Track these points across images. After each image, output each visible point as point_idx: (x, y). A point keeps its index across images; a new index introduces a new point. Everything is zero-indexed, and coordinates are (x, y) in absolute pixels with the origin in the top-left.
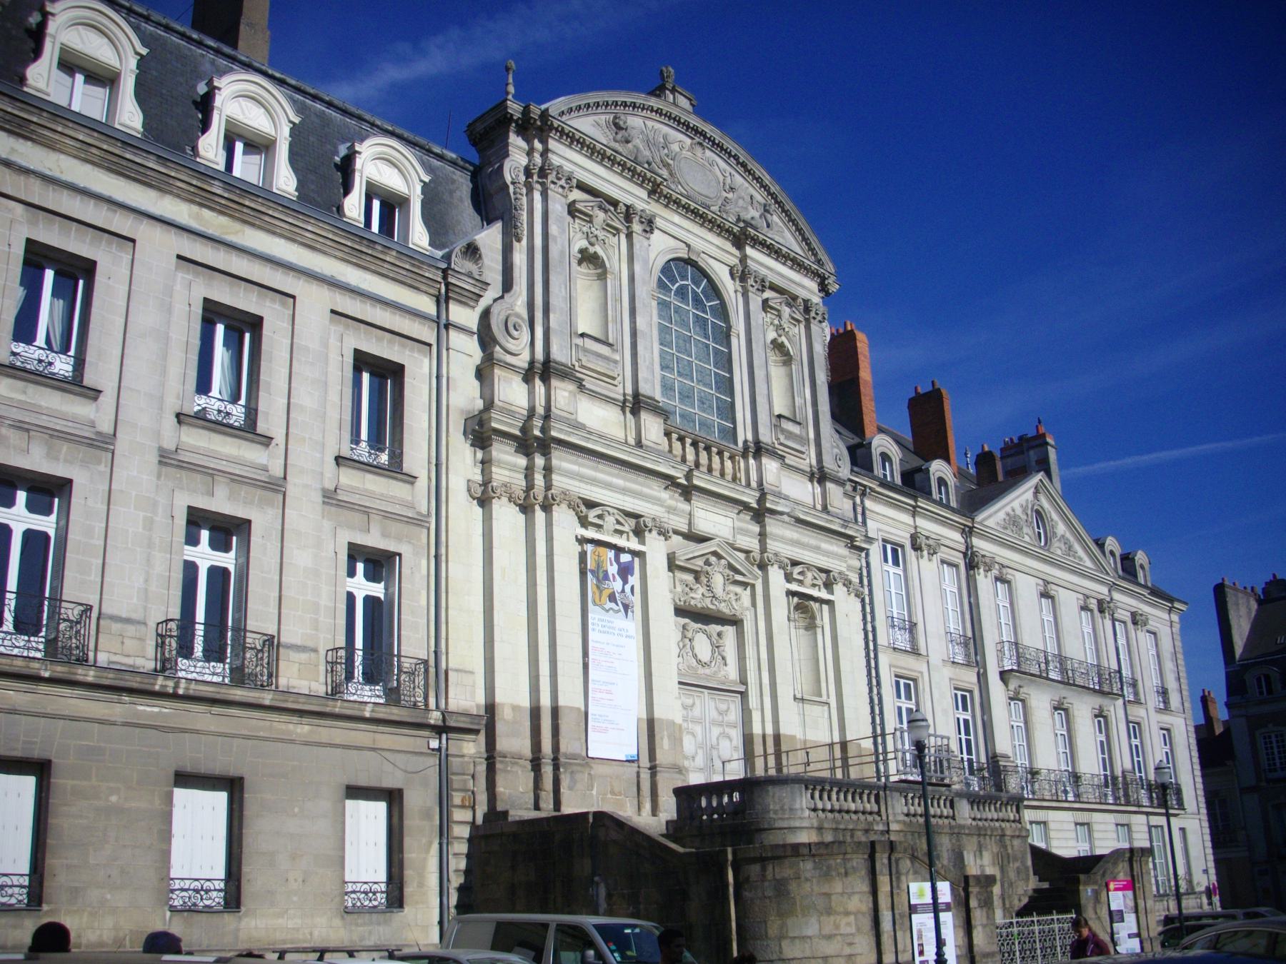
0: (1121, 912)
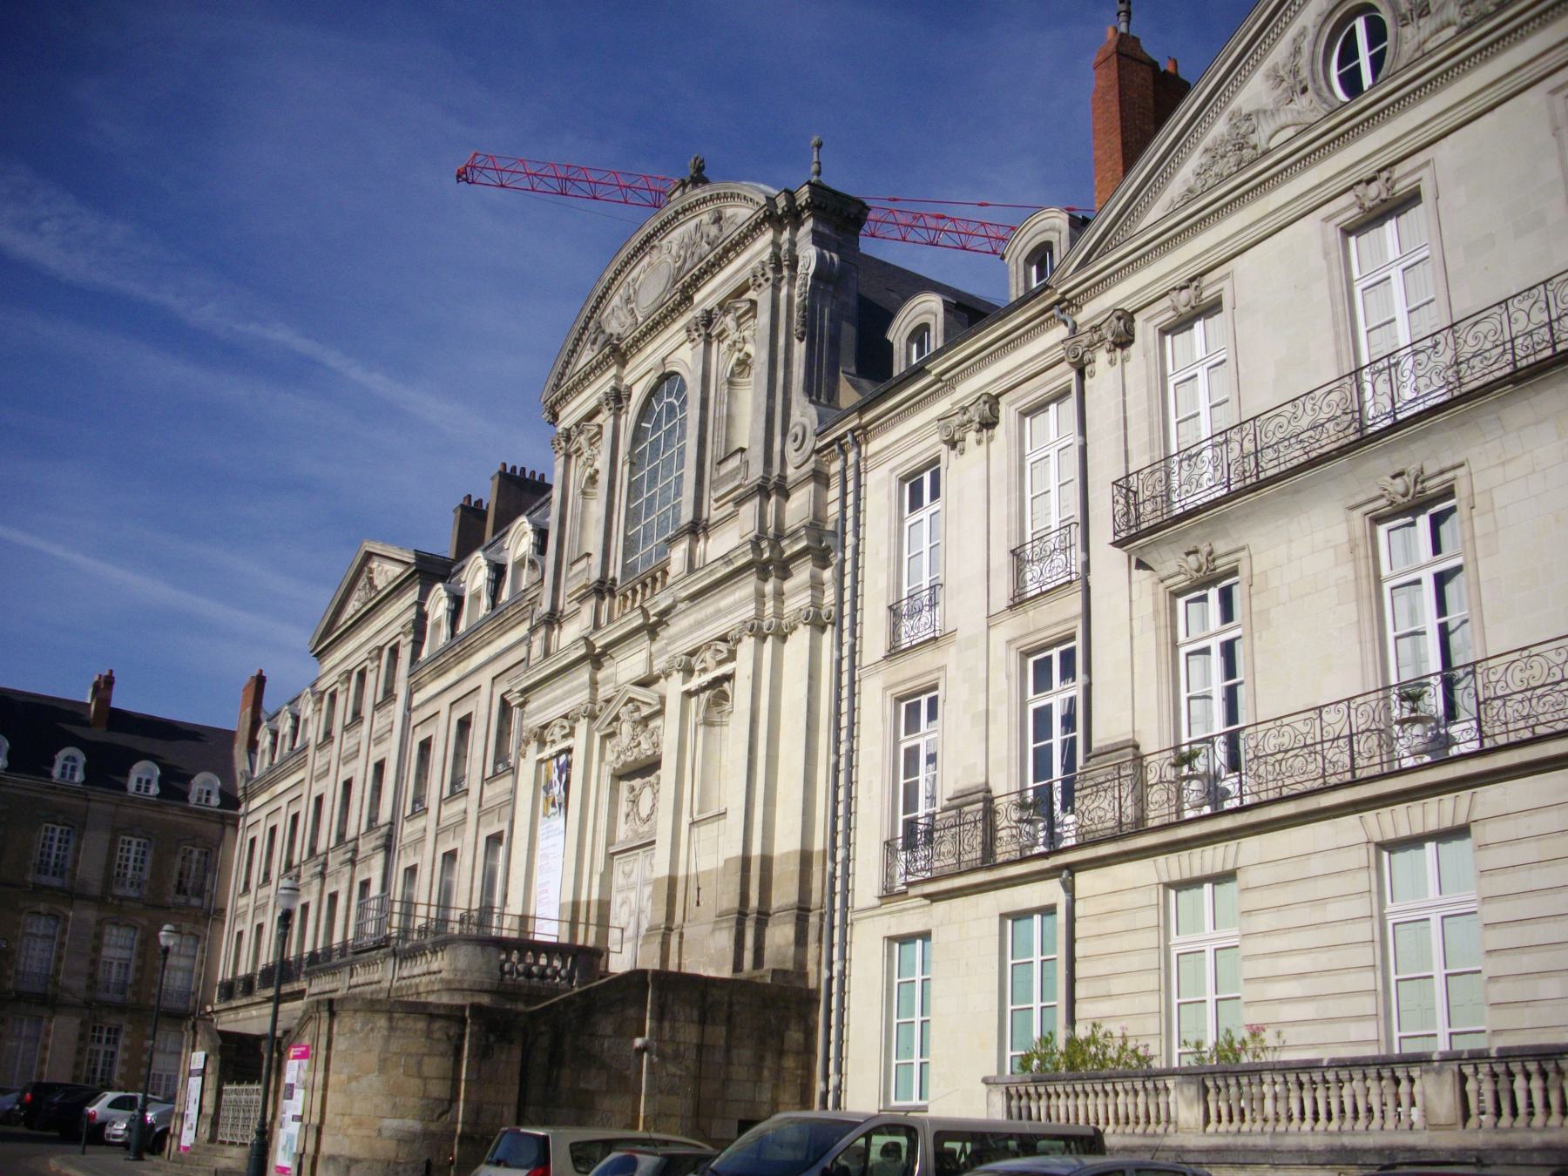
0: (292, 1086)
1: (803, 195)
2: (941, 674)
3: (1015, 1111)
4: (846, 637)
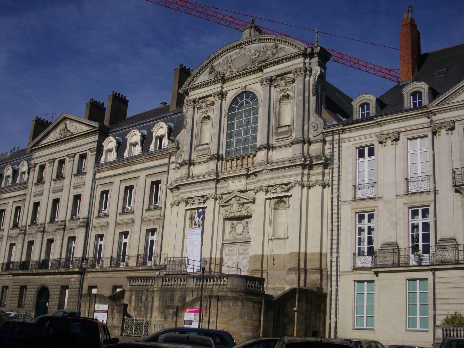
1: (317, 50)
2: (376, 208)
3: (445, 334)
4: (335, 191)
